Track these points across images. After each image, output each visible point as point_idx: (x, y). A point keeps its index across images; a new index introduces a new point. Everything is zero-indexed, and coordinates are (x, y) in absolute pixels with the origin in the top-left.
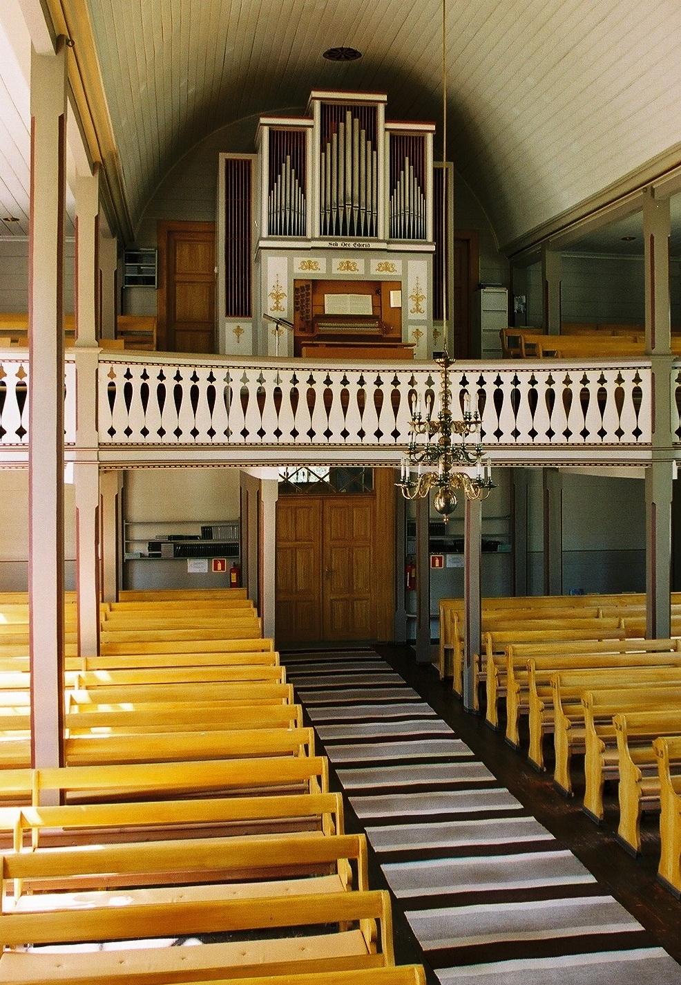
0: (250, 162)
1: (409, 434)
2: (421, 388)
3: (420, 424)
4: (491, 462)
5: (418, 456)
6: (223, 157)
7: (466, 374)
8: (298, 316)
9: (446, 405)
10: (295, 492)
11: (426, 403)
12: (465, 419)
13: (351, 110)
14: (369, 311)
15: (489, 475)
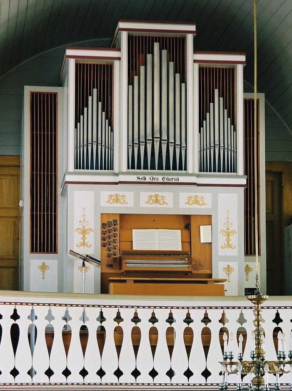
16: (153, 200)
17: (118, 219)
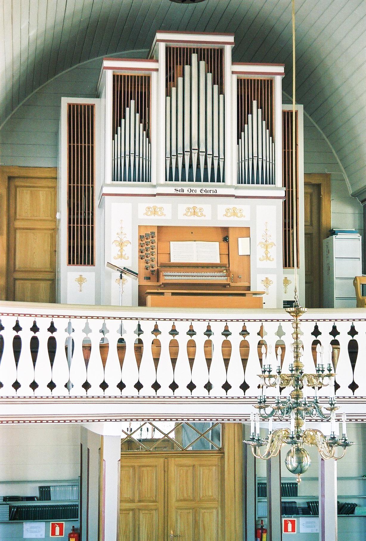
0: (93, 106)
1: (259, 387)
2: (271, 339)
3: (270, 377)
4: (346, 418)
5: (269, 410)
6: (65, 102)
7: (319, 324)
8: (144, 265)
9: (297, 357)
10: (138, 449)
11: (277, 355)
12: (318, 371)
13: (197, 53)
14: (216, 260)
15: (345, 432)
16: (191, 212)
17: (156, 231)
